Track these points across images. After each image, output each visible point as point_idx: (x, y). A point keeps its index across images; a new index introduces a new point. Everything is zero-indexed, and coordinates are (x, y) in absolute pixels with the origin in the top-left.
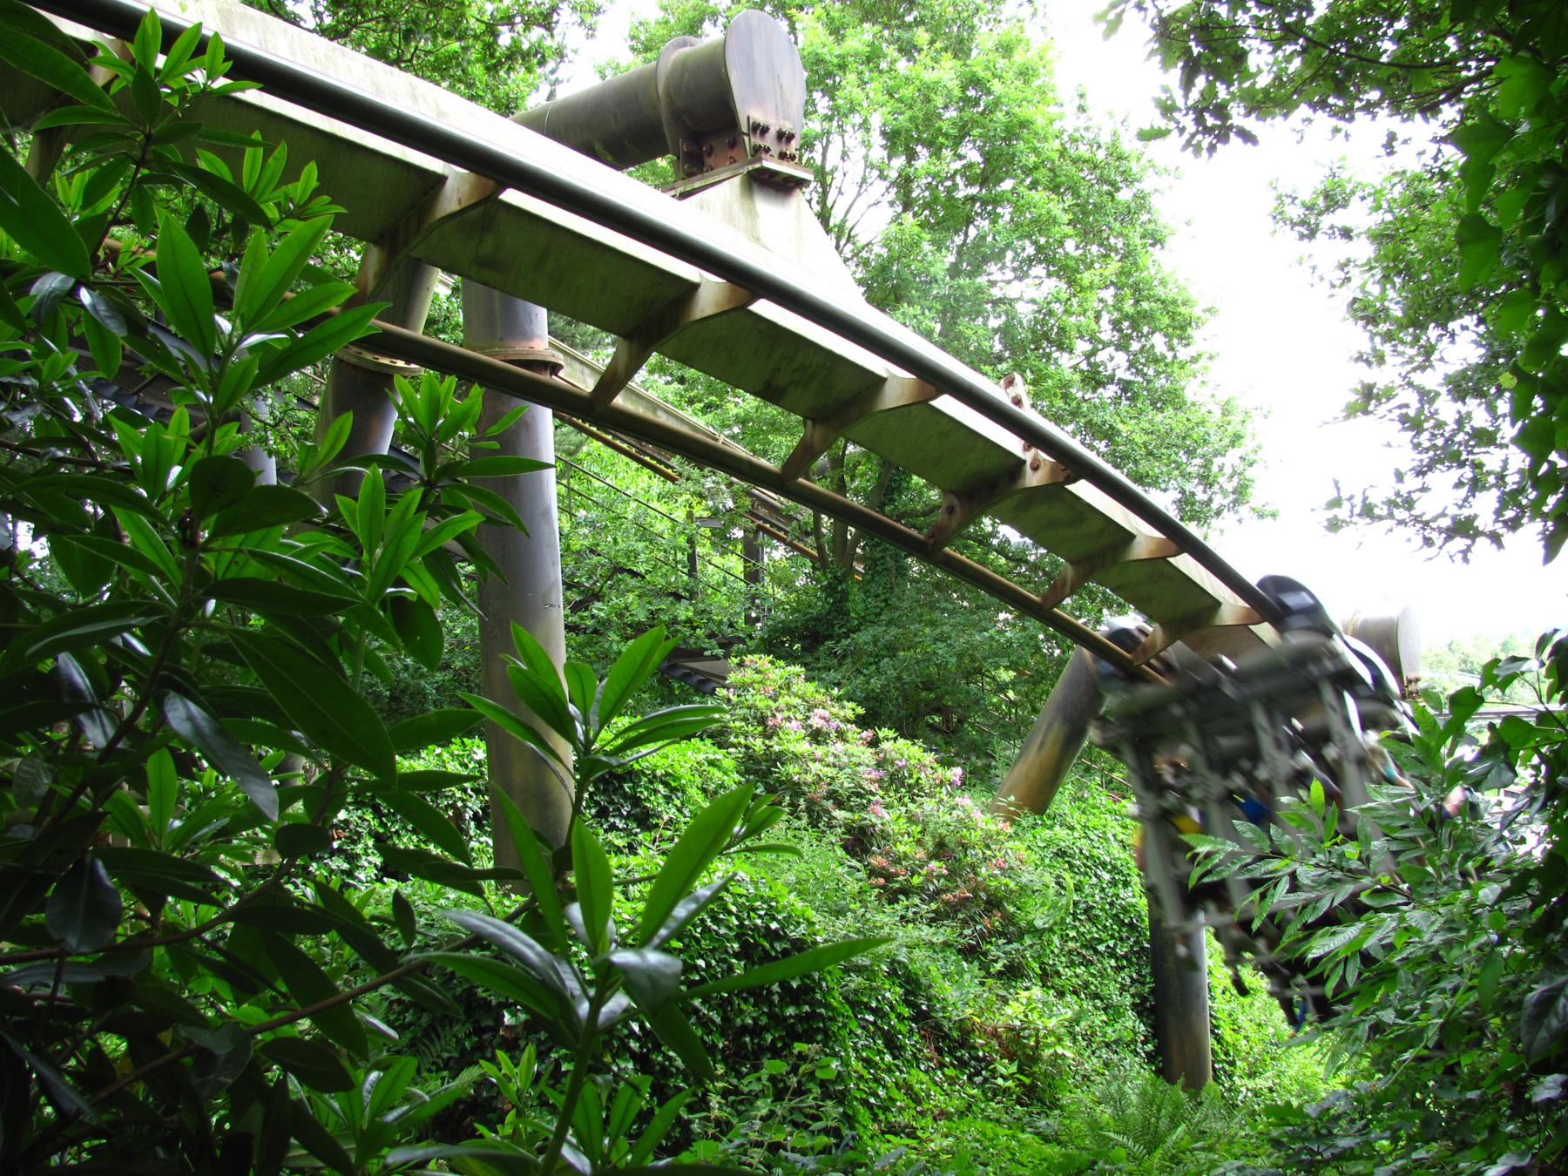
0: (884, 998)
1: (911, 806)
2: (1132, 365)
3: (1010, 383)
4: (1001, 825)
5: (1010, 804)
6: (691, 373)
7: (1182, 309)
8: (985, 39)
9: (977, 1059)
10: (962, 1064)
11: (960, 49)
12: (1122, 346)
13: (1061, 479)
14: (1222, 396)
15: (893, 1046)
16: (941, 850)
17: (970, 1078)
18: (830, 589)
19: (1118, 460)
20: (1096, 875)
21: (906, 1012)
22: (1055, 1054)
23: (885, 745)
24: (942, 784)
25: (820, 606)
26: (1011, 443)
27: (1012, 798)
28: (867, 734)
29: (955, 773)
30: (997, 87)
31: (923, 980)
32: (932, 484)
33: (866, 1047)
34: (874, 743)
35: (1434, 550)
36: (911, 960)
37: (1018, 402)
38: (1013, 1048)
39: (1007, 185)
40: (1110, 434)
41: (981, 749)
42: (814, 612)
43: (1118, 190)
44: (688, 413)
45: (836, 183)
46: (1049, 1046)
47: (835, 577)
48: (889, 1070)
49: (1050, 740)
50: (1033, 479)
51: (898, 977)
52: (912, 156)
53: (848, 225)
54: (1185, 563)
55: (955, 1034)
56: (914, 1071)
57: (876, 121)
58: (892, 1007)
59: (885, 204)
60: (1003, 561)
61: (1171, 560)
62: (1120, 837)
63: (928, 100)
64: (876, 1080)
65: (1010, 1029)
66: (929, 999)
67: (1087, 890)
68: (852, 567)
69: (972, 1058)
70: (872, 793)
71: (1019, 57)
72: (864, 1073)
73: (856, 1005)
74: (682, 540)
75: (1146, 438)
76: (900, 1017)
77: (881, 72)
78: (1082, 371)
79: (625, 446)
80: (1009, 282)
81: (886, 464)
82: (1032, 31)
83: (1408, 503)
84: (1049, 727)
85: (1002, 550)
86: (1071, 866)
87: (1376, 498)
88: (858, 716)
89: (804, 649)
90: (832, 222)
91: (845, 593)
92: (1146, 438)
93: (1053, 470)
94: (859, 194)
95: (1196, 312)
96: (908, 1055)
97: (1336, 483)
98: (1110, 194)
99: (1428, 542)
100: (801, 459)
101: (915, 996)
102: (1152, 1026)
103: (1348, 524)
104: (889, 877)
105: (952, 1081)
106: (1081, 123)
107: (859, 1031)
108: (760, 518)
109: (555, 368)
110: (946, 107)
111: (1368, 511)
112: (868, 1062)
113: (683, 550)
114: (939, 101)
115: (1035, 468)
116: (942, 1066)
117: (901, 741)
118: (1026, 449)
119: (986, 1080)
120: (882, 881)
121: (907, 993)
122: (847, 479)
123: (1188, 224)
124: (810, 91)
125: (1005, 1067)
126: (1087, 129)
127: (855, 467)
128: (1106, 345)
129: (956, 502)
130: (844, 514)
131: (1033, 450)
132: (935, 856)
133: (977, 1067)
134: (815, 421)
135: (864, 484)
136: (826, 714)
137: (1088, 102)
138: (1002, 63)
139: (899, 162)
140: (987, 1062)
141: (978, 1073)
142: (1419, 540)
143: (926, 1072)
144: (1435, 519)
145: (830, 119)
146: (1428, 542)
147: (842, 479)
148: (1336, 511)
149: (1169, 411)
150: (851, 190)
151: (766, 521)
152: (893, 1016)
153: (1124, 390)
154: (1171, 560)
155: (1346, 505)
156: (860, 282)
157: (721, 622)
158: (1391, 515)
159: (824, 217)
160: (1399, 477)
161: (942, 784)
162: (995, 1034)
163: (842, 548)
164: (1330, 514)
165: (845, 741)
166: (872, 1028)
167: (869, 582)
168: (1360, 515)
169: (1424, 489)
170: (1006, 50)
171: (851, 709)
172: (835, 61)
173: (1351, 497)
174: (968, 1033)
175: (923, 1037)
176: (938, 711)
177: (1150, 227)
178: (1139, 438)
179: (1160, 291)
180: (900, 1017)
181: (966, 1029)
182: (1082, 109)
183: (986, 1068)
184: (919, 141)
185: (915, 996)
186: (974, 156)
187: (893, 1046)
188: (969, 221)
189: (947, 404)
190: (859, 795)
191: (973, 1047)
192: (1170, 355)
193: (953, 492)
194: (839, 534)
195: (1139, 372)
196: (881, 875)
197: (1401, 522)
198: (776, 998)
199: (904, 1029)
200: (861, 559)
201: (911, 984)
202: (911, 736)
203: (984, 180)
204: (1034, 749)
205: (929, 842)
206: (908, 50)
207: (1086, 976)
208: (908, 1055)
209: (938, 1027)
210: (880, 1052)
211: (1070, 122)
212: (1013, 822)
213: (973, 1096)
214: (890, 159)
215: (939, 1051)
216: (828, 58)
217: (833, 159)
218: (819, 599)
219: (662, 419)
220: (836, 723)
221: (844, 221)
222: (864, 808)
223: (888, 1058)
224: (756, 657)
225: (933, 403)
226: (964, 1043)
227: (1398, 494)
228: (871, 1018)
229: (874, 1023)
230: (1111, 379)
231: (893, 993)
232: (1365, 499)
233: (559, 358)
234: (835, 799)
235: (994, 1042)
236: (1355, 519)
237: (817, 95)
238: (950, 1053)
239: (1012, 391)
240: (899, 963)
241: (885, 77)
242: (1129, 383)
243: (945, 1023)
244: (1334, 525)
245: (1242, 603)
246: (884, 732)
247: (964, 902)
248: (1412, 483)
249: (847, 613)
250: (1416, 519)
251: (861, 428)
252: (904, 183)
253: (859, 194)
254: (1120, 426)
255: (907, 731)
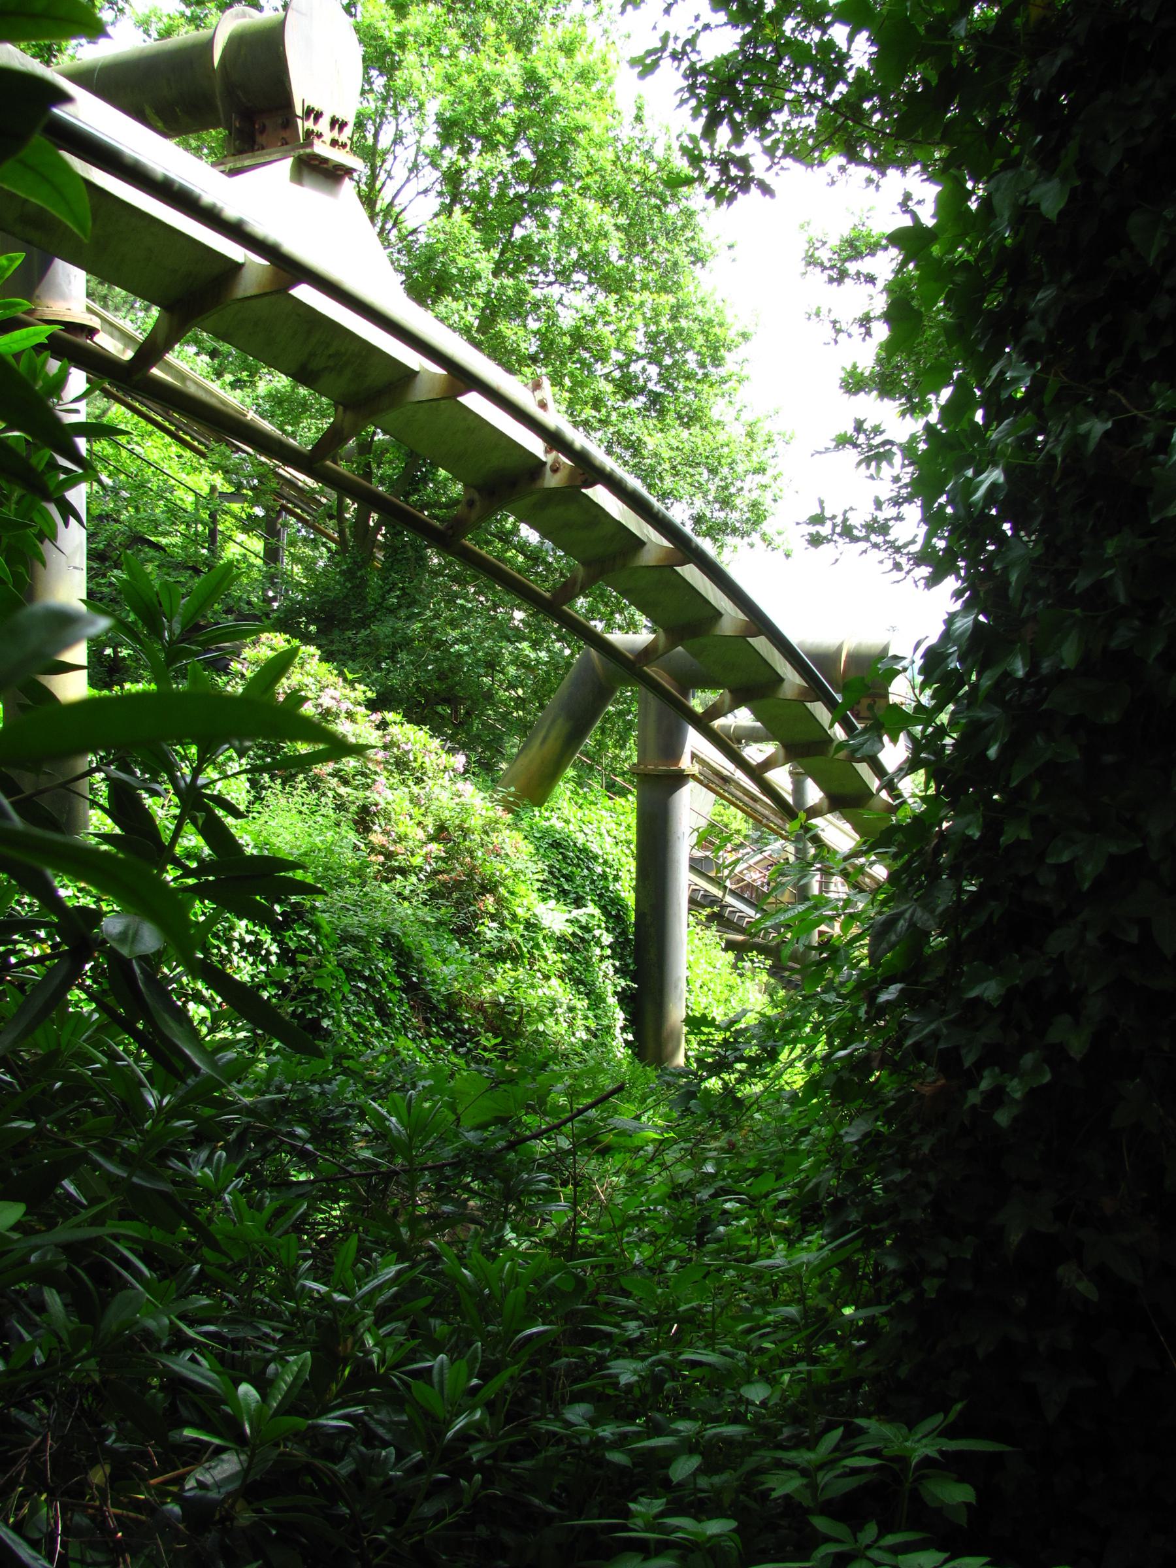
0: (377, 968)
1: (416, 790)
2: (662, 378)
3: (537, 386)
4: (500, 813)
5: (510, 795)
6: (225, 347)
7: (716, 330)
8: (547, 35)
9: (463, 1031)
10: (448, 1035)
11: (522, 41)
12: (654, 359)
13: (579, 483)
14: (747, 417)
15: (383, 1013)
16: (441, 833)
17: (454, 1049)
18: (349, 574)
19: (647, 475)
20: (588, 868)
21: (397, 982)
22: (537, 1031)
23: (393, 729)
24: (445, 770)
25: (336, 592)
26: (534, 445)
27: (512, 789)
28: (377, 717)
29: (459, 760)
30: (556, 88)
31: (415, 955)
32: (457, 477)
33: (358, 1013)
34: (383, 725)
35: (902, 574)
36: (405, 934)
37: (543, 405)
38: (497, 1022)
39: (558, 187)
40: (635, 447)
41: (495, 745)
42: (332, 595)
43: (666, 204)
44: (215, 386)
45: (387, 166)
46: (530, 1023)
47: (355, 563)
48: (378, 1035)
49: (554, 734)
50: (552, 481)
51: (392, 949)
52: (465, 151)
53: (397, 209)
54: (691, 573)
55: (443, 1007)
56: (401, 1038)
57: (433, 108)
58: (384, 977)
59: (433, 194)
60: (521, 558)
61: (678, 569)
62: (614, 833)
63: (487, 93)
64: (366, 1044)
65: (496, 1004)
66: (420, 972)
67: (578, 881)
68: (372, 553)
69: (457, 1030)
70: (376, 773)
71: (581, 58)
72: (355, 1036)
73: (351, 973)
74: (205, 515)
75: (672, 454)
76: (391, 987)
77: (441, 56)
78: (613, 381)
79: (144, 409)
80: (551, 284)
81: (413, 457)
82: (592, 31)
83: (884, 529)
84: (554, 721)
85: (523, 548)
86: (565, 857)
87: (856, 520)
88: (369, 700)
89: (319, 631)
90: (380, 205)
91: (364, 582)
92: (672, 454)
93: (572, 474)
94: (408, 180)
95: (731, 335)
96: (397, 1023)
97: (821, 502)
98: (658, 207)
99: (897, 566)
100: (330, 442)
101: (407, 968)
102: (630, 1014)
103: (829, 541)
104: (390, 856)
105: (437, 1049)
106: (637, 133)
107: (352, 997)
108: (284, 498)
109: (91, 332)
110: (504, 104)
111: (847, 532)
112: (358, 1026)
113: (205, 524)
114: (498, 95)
115: (555, 470)
116: (428, 1035)
117: (408, 726)
118: (547, 452)
119: (470, 1050)
120: (381, 858)
121: (399, 965)
122: (374, 466)
123: (730, 247)
124: (366, 69)
125: (488, 1040)
126: (640, 140)
127: (382, 454)
128: (640, 358)
129: (476, 496)
130: (369, 500)
131: (554, 453)
132: (432, 839)
133: (461, 1038)
134: (346, 408)
135: (390, 472)
136: (337, 694)
137: (646, 114)
138: (562, 60)
139: (450, 154)
140: (472, 1034)
141: (463, 1045)
142: (889, 564)
143: (413, 1040)
144: (906, 545)
145: (385, 100)
146: (897, 566)
147: (368, 465)
148: (818, 528)
149: (696, 429)
150: (400, 172)
151: (289, 501)
152: (384, 985)
153: (654, 403)
154: (678, 569)
155: (829, 524)
156: (399, 270)
157: (240, 598)
158: (866, 539)
159: (368, 201)
160: (878, 504)
161: (445, 770)
162: (480, 1008)
163: (363, 532)
164: (813, 529)
165: (354, 721)
166: (364, 996)
167: (388, 570)
168: (840, 535)
169: (899, 518)
170: (568, 49)
171: (362, 692)
172: (394, 37)
173: (834, 517)
174: (456, 1006)
175: (412, 1007)
176: (447, 701)
177: (693, 245)
178: (666, 453)
179: (698, 311)
180: (391, 987)
181: (453, 1002)
182: (639, 119)
183: (470, 1041)
184: (474, 133)
185: (407, 968)
186: (527, 155)
187: (383, 1013)
188: (516, 221)
189: (473, 401)
190: (363, 774)
191: (460, 1021)
192: (700, 372)
193: (475, 487)
194: (362, 516)
195: (669, 386)
196: (381, 853)
197: (876, 546)
198: (274, 959)
199: (395, 998)
200: (383, 547)
201: (404, 956)
202: (418, 721)
203: (534, 180)
204: (537, 742)
205: (429, 822)
206: (472, 38)
207: (571, 962)
208: (397, 1023)
209: (427, 998)
210: (370, 1018)
211: (627, 132)
212: (510, 811)
213: (455, 1065)
214: (443, 148)
215: (427, 1021)
216: (387, 34)
217: (385, 141)
218: (338, 582)
219: (192, 389)
220: (346, 705)
221: (391, 205)
222: (367, 787)
223: (377, 1024)
224: (272, 635)
225: (460, 399)
226: (451, 1016)
227: (875, 520)
228: (363, 986)
229: (366, 991)
230: (642, 390)
231: (386, 963)
232: (845, 520)
233: (94, 322)
234: (341, 777)
235: (480, 1017)
236: (836, 537)
237: (374, 73)
238: (437, 1024)
239: (539, 395)
240: (393, 935)
241: (446, 63)
242: (658, 395)
243: (434, 995)
244: (816, 541)
245: (741, 616)
246: (390, 716)
247: (458, 884)
248: (889, 512)
249: (364, 599)
250: (891, 544)
251: (391, 416)
252: (453, 178)
253: (408, 180)
254: (646, 438)
255: (415, 717)
